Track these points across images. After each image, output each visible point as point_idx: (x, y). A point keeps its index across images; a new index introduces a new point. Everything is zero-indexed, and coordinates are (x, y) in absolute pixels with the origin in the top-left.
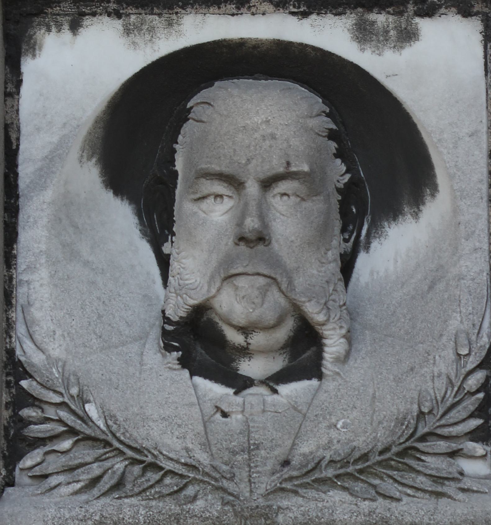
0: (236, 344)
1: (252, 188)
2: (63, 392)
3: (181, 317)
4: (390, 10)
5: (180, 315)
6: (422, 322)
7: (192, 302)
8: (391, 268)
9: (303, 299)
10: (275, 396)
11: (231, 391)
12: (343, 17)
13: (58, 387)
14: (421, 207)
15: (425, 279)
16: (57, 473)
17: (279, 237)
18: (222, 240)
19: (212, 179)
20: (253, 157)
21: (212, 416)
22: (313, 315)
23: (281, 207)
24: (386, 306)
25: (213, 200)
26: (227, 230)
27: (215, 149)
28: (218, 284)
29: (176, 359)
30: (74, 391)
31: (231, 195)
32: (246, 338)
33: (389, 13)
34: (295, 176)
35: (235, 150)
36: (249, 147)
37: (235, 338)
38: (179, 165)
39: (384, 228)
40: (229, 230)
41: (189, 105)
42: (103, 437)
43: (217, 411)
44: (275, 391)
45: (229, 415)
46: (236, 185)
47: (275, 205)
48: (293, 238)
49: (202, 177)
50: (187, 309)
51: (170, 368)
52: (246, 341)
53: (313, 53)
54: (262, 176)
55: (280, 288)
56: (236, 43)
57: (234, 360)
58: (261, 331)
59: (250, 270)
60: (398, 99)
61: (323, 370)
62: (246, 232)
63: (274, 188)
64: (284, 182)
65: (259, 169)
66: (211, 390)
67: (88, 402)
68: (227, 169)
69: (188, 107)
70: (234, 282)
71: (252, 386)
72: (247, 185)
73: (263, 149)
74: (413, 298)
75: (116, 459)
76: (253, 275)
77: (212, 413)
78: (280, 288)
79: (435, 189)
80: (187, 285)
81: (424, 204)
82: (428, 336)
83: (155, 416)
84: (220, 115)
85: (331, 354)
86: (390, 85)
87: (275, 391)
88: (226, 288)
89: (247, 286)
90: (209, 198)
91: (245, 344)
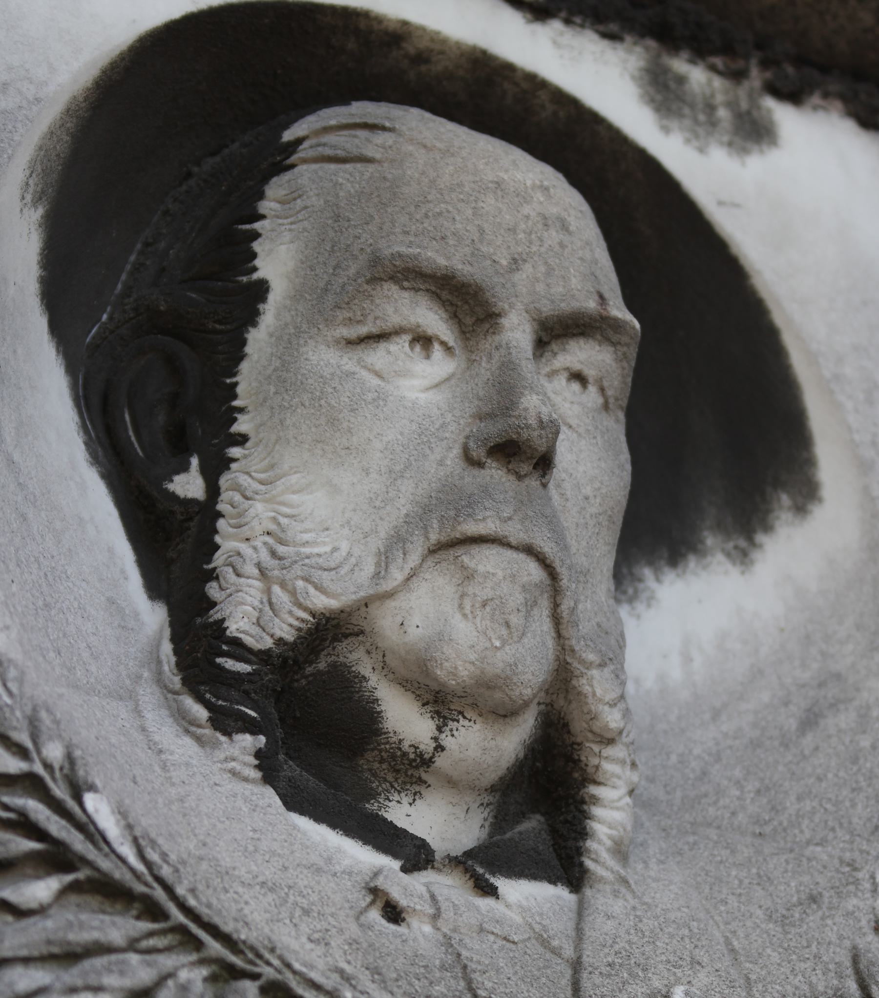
0: (405, 746)
1: (517, 332)
2: (29, 745)
3: (280, 641)
4: (718, 61)
5: (279, 633)
6: (799, 799)
7: (321, 602)
8: (676, 674)
9: (591, 657)
10: (486, 903)
11: (396, 865)
12: (618, 45)
13: (15, 728)
14: (760, 538)
15: (786, 704)
16: (26, 961)
17: (564, 475)
18: (431, 448)
19: (417, 290)
20: (524, 256)
21: (361, 913)
22: (601, 707)
23: (567, 405)
24: (674, 758)
25: (407, 345)
26: (443, 425)
27: (426, 216)
28: (414, 559)
29: (253, 751)
30: (54, 752)
31: (451, 343)
32: (439, 729)
33: (713, 68)
34: (610, 333)
35: (481, 231)
36: (513, 230)
37: (405, 720)
38: (276, 260)
39: (640, 580)
40: (450, 428)
41: (288, 136)
42: (140, 888)
43: (373, 903)
44: (490, 891)
45: (403, 920)
46: (469, 321)
47: (553, 396)
48: (588, 491)
49: (392, 278)
50: (303, 621)
51: (234, 773)
52: (436, 739)
53: (550, 108)
54: (547, 309)
55: (556, 606)
56: (386, 33)
57: (373, 795)
58: (479, 720)
59: (515, 532)
60: (743, 261)
61: (589, 863)
62: (528, 426)
63: (555, 354)
64: (582, 341)
65: (540, 287)
66: (339, 850)
67: (92, 788)
68: (467, 269)
69: (288, 136)
70: (466, 559)
71: (426, 869)
72: (505, 322)
73: (546, 245)
74: (755, 744)
75: (174, 957)
76: (516, 548)
77: (364, 904)
78: (556, 606)
79: (806, 493)
80: (308, 557)
81: (768, 528)
82: (833, 829)
83: (247, 878)
84: (425, 147)
85: (610, 828)
86: (729, 224)
87: (490, 891)
88: (427, 576)
89: (500, 574)
90: (396, 339)
91: (427, 746)
